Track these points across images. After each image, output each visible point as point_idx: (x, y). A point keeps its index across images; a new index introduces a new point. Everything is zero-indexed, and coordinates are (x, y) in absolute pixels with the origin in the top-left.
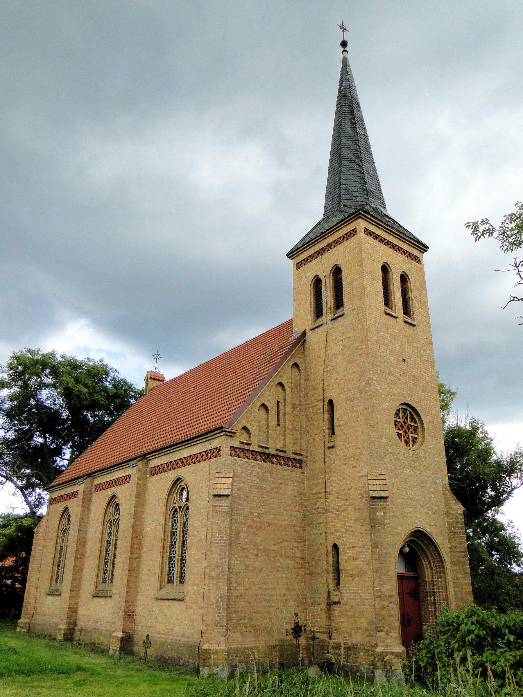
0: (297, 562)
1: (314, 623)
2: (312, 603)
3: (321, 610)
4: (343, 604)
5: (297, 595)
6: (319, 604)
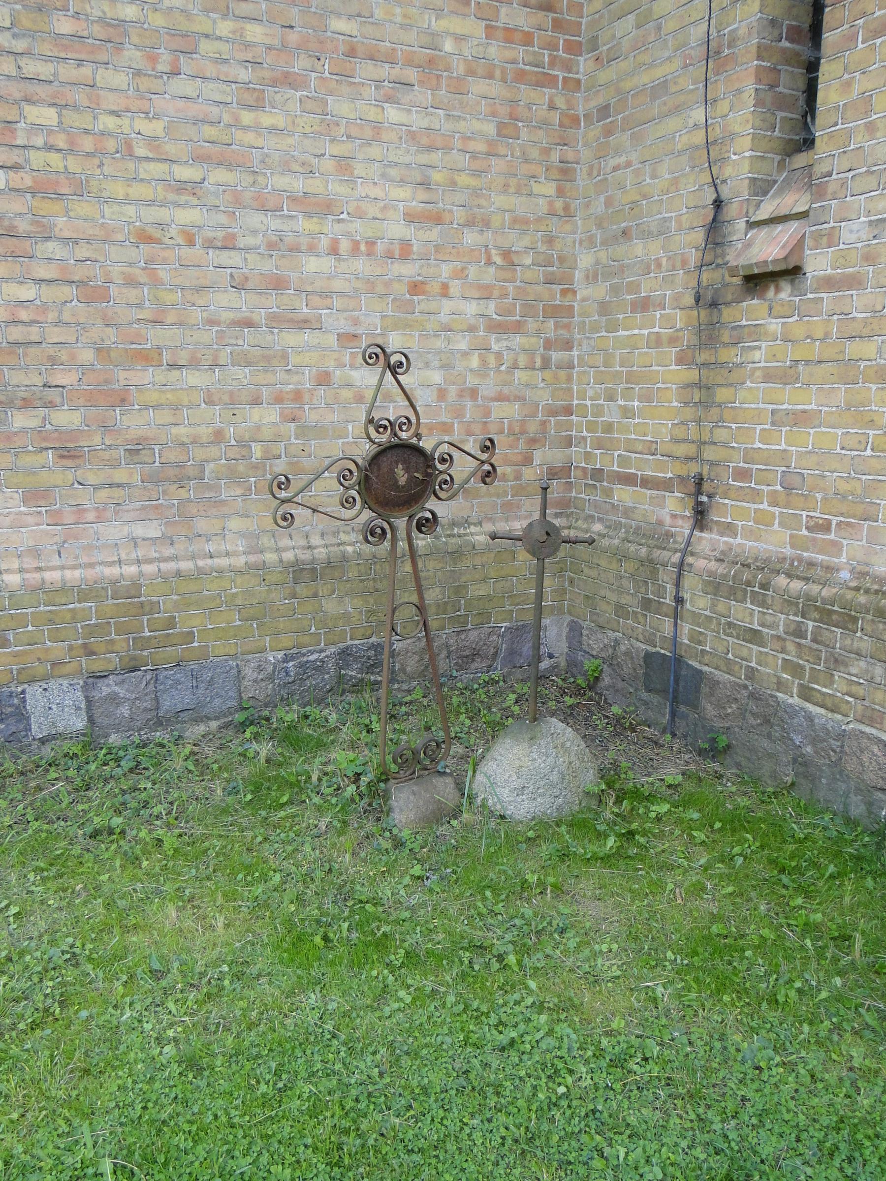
0: (509, 35)
1: (609, 428)
2: (604, 308)
3: (657, 341)
4: (828, 283)
5: (507, 254)
6: (644, 305)
